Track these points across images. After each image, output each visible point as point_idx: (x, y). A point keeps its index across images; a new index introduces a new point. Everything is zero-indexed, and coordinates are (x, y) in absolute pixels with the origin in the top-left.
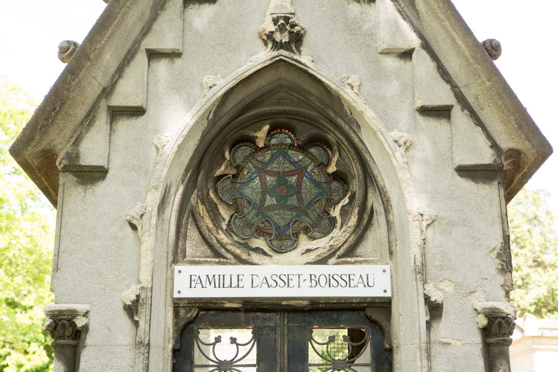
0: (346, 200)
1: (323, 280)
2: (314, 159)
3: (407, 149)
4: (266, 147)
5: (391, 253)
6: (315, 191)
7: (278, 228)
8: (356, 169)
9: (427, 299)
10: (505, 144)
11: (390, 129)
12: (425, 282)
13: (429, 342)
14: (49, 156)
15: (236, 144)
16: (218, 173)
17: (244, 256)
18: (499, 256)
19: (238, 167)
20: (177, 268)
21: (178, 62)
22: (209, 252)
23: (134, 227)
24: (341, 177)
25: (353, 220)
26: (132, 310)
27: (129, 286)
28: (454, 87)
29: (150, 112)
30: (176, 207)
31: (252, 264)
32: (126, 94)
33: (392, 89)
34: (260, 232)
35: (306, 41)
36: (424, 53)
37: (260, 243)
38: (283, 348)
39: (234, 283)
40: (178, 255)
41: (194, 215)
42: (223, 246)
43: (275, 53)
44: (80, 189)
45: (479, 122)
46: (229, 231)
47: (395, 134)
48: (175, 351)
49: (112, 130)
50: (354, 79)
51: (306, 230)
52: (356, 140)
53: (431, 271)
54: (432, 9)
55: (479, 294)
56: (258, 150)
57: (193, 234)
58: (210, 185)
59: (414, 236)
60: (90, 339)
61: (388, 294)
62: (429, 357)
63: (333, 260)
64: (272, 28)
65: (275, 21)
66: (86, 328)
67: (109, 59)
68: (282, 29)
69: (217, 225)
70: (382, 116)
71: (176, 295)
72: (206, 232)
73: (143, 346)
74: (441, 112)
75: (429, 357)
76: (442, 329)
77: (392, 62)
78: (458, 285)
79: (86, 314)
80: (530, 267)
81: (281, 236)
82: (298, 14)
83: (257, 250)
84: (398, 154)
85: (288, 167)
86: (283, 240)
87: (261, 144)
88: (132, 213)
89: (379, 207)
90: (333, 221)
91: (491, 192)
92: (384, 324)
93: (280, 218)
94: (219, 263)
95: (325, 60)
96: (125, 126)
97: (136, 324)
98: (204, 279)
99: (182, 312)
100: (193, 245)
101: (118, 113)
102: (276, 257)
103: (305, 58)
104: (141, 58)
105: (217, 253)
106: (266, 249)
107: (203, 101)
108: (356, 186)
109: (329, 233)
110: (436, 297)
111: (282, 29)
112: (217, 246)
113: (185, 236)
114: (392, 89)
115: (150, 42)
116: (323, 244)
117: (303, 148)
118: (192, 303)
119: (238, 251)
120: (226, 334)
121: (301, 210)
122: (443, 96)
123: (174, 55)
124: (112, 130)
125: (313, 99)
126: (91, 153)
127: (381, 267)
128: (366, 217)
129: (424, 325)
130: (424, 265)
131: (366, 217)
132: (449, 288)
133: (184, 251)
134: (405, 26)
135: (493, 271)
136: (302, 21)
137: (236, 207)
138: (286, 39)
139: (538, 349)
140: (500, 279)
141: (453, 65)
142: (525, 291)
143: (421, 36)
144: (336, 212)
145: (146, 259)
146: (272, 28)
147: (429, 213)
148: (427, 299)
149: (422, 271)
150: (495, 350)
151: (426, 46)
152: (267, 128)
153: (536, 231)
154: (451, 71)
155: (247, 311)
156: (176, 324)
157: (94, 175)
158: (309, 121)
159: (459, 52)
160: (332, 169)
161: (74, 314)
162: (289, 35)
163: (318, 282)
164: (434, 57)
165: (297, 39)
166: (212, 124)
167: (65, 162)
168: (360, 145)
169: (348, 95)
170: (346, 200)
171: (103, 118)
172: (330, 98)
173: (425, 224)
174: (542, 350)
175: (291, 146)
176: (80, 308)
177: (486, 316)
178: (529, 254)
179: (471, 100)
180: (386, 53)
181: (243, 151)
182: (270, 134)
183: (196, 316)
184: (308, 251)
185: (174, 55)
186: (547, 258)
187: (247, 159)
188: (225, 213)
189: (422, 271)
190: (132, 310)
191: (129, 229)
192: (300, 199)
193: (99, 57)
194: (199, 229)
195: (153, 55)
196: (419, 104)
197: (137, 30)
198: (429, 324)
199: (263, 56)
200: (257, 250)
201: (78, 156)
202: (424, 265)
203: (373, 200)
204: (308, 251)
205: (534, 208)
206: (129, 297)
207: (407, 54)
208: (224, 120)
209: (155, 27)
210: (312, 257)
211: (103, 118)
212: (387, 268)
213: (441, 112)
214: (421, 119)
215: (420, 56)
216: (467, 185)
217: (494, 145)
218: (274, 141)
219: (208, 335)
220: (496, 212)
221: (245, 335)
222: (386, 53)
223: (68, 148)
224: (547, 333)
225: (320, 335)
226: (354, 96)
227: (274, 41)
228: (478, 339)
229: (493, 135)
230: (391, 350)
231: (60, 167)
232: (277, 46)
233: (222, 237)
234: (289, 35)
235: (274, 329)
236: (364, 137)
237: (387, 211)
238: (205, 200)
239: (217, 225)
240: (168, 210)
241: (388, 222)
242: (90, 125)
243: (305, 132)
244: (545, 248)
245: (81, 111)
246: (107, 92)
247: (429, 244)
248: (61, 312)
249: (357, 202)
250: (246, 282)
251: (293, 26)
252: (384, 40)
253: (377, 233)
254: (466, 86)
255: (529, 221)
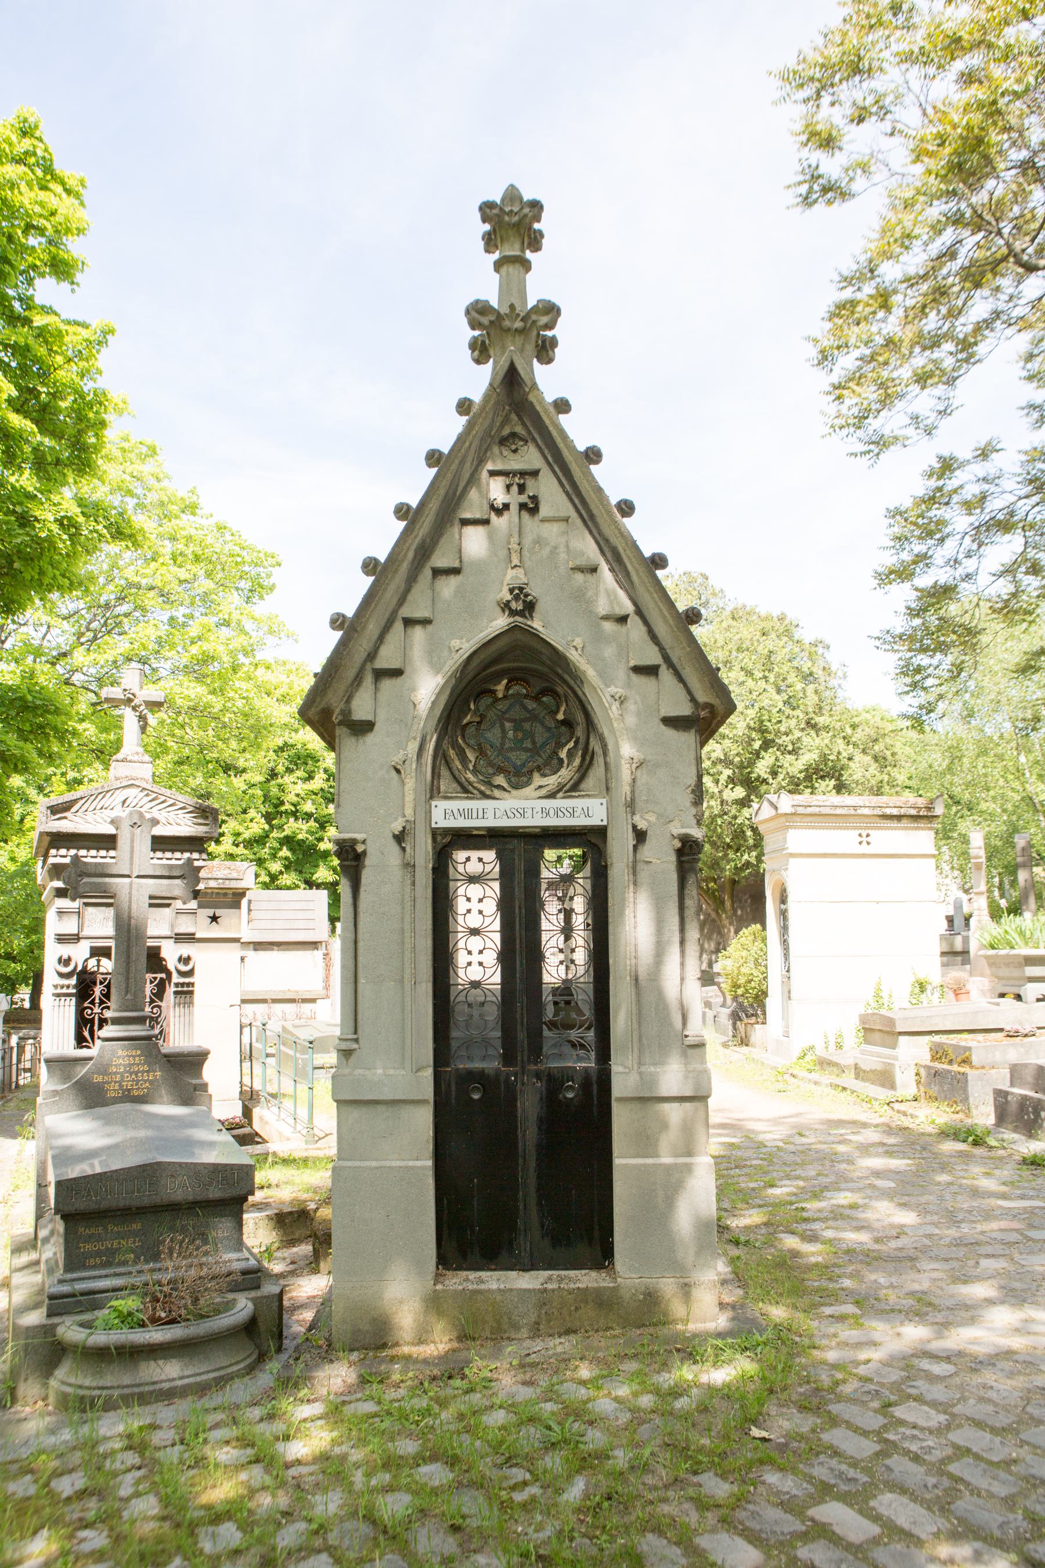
0: (571, 744)
1: (552, 812)
2: (546, 707)
3: (622, 703)
4: (505, 697)
5: (608, 789)
6: (547, 735)
7: (515, 766)
8: (580, 717)
9: (634, 827)
10: (702, 697)
11: (608, 686)
12: (633, 814)
13: (635, 862)
14: (327, 713)
15: (478, 697)
16: (465, 721)
17: (488, 792)
18: (693, 792)
19: (481, 716)
20: (434, 803)
21: (430, 628)
22: (459, 789)
23: (398, 771)
24: (568, 723)
25: (577, 761)
26: (400, 838)
27: (396, 819)
28: (662, 649)
29: (408, 671)
30: (431, 752)
31: (494, 798)
32: (386, 659)
33: (609, 652)
34: (500, 770)
35: (538, 608)
36: (637, 619)
37: (500, 780)
38: (520, 866)
39: (481, 815)
40: (434, 792)
41: (445, 757)
42: (470, 784)
43: (512, 620)
44: (353, 739)
45: (681, 679)
46: (475, 771)
47: (612, 690)
48: (435, 870)
49: (376, 689)
50: (578, 642)
51: (539, 769)
52: (580, 693)
53: (639, 804)
54: (643, 582)
55: (676, 823)
56: (497, 700)
57: (444, 772)
58: (459, 732)
59: (626, 774)
60: (368, 861)
61: (605, 823)
62: (635, 873)
63: (561, 794)
64: (509, 597)
65: (511, 591)
66: (364, 852)
67: (373, 628)
68: (517, 598)
69: (466, 768)
70: (601, 674)
71: (434, 825)
72: (456, 772)
73: (409, 866)
74: (649, 671)
75: (635, 873)
76: (647, 852)
77: (608, 626)
78: (660, 816)
79: (364, 842)
80: (803, 730)
81: (518, 774)
82: (532, 584)
83: (499, 787)
84: (614, 708)
85: (524, 715)
86: (519, 778)
87: (500, 695)
88: (395, 759)
89: (598, 750)
90: (561, 761)
91: (688, 738)
92: (601, 846)
93: (518, 757)
94: (468, 798)
95: (551, 625)
96: (387, 684)
97: (404, 849)
98: (456, 812)
99: (439, 838)
100: (446, 783)
101: (380, 674)
102: (514, 792)
103: (537, 624)
104: (399, 625)
105: (466, 790)
106: (506, 785)
107: (450, 662)
108: (580, 732)
109: (558, 770)
110: (642, 825)
111: (517, 598)
112: (466, 784)
113: (439, 776)
114: (609, 652)
115: (406, 612)
116: (552, 781)
117: (536, 698)
118: (446, 831)
119: (483, 788)
120: (475, 855)
121: (535, 751)
122: (651, 656)
123: (426, 622)
124: (376, 689)
125: (544, 658)
126: (361, 709)
127: (598, 801)
128: (588, 758)
129: (631, 848)
130: (633, 800)
131: (588, 758)
132: (652, 818)
133: (439, 788)
134: (621, 594)
135: (688, 804)
136: (534, 591)
137: (481, 752)
138: (520, 607)
139: (791, 827)
140: (693, 811)
141: (662, 630)
142: (794, 757)
143: (635, 604)
144: (563, 754)
145: (409, 798)
146: (509, 597)
147: (638, 756)
148: (634, 827)
149: (631, 806)
150: (687, 866)
151: (639, 612)
152: (505, 682)
153: (811, 688)
154: (659, 635)
155: (490, 837)
156: (434, 848)
157: (363, 728)
158: (541, 676)
159: (665, 621)
160: (560, 716)
161: (354, 841)
162: (522, 603)
163: (548, 814)
164: (646, 622)
165: (530, 607)
166: (459, 680)
167: (340, 718)
168: (583, 698)
169: (573, 656)
170: (571, 744)
171: (369, 679)
172: (558, 659)
173: (634, 766)
174: (795, 827)
175: (526, 696)
176: (359, 836)
177: (680, 840)
178: (801, 716)
179: (675, 660)
180: (606, 618)
181: (486, 701)
182: (507, 688)
183: (451, 841)
184: (540, 787)
185: (426, 622)
186: (821, 720)
187: (488, 707)
188: (471, 756)
189: (631, 806)
190: (400, 838)
191: (394, 773)
192: (534, 742)
193: (364, 628)
194: (450, 769)
195: (409, 622)
196: (632, 663)
197: (395, 600)
198: (635, 848)
199: (501, 622)
200: (499, 787)
201: (350, 712)
202: (633, 800)
203: (594, 744)
204: (540, 787)
205: (810, 664)
206: (397, 827)
207: (623, 619)
208: (469, 677)
209: (410, 597)
210: (543, 792)
211: (369, 679)
212: (604, 801)
213: (649, 671)
214: (634, 677)
215: (634, 621)
216: (670, 733)
217: (693, 700)
218: (511, 692)
219: (460, 856)
220: (692, 755)
221: (490, 855)
222: (606, 618)
223: (342, 705)
224: (801, 810)
225: (550, 854)
226: (577, 657)
227: (510, 609)
228: (673, 858)
229: (693, 690)
230: (606, 866)
231: (336, 721)
232: (513, 613)
233: (469, 776)
234: (522, 603)
235: (513, 851)
236: (586, 691)
237: (605, 754)
238: (455, 745)
239: (466, 768)
240: (425, 754)
241: (606, 763)
242: (359, 685)
243: (538, 685)
244: (819, 710)
245: (351, 674)
246: (372, 656)
247: (638, 783)
248: (344, 840)
249: (581, 746)
250: (490, 814)
251: (526, 595)
252: (602, 607)
253: (597, 771)
254: (672, 648)
255: (805, 678)
